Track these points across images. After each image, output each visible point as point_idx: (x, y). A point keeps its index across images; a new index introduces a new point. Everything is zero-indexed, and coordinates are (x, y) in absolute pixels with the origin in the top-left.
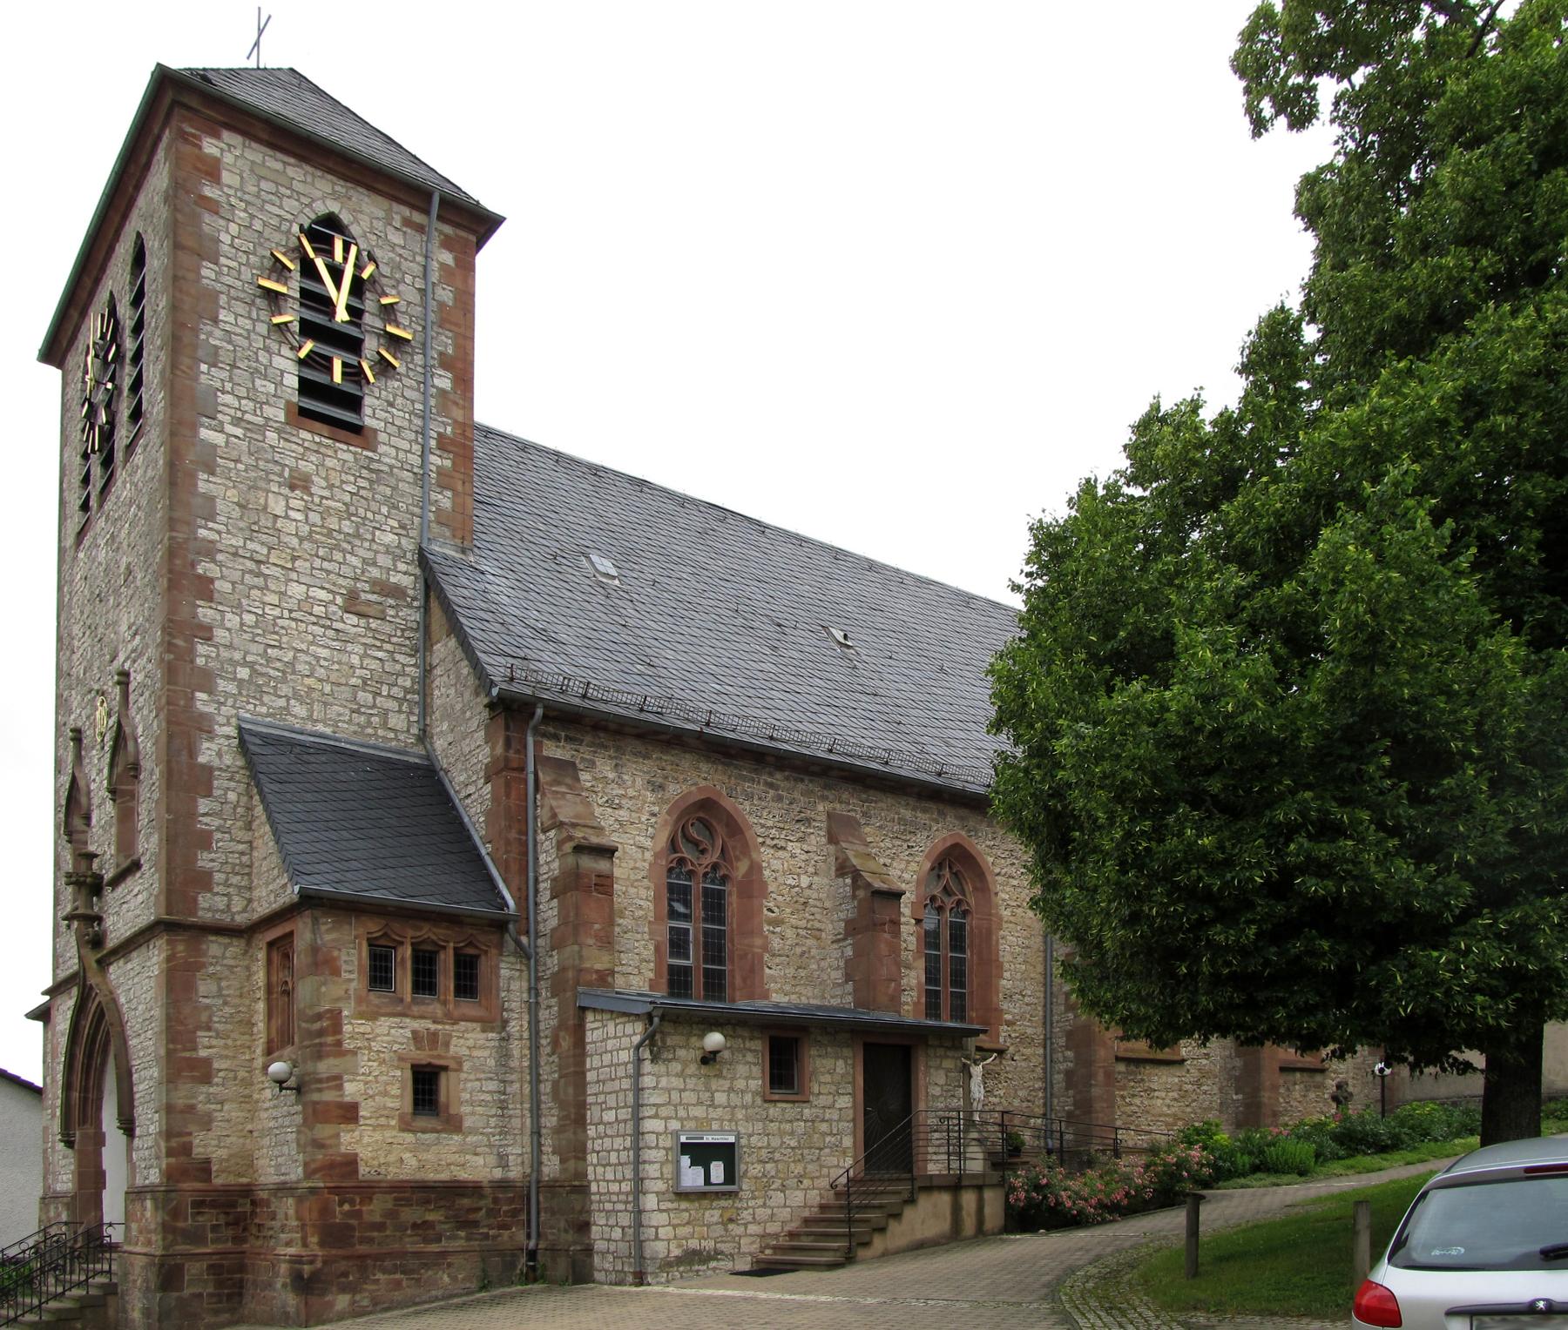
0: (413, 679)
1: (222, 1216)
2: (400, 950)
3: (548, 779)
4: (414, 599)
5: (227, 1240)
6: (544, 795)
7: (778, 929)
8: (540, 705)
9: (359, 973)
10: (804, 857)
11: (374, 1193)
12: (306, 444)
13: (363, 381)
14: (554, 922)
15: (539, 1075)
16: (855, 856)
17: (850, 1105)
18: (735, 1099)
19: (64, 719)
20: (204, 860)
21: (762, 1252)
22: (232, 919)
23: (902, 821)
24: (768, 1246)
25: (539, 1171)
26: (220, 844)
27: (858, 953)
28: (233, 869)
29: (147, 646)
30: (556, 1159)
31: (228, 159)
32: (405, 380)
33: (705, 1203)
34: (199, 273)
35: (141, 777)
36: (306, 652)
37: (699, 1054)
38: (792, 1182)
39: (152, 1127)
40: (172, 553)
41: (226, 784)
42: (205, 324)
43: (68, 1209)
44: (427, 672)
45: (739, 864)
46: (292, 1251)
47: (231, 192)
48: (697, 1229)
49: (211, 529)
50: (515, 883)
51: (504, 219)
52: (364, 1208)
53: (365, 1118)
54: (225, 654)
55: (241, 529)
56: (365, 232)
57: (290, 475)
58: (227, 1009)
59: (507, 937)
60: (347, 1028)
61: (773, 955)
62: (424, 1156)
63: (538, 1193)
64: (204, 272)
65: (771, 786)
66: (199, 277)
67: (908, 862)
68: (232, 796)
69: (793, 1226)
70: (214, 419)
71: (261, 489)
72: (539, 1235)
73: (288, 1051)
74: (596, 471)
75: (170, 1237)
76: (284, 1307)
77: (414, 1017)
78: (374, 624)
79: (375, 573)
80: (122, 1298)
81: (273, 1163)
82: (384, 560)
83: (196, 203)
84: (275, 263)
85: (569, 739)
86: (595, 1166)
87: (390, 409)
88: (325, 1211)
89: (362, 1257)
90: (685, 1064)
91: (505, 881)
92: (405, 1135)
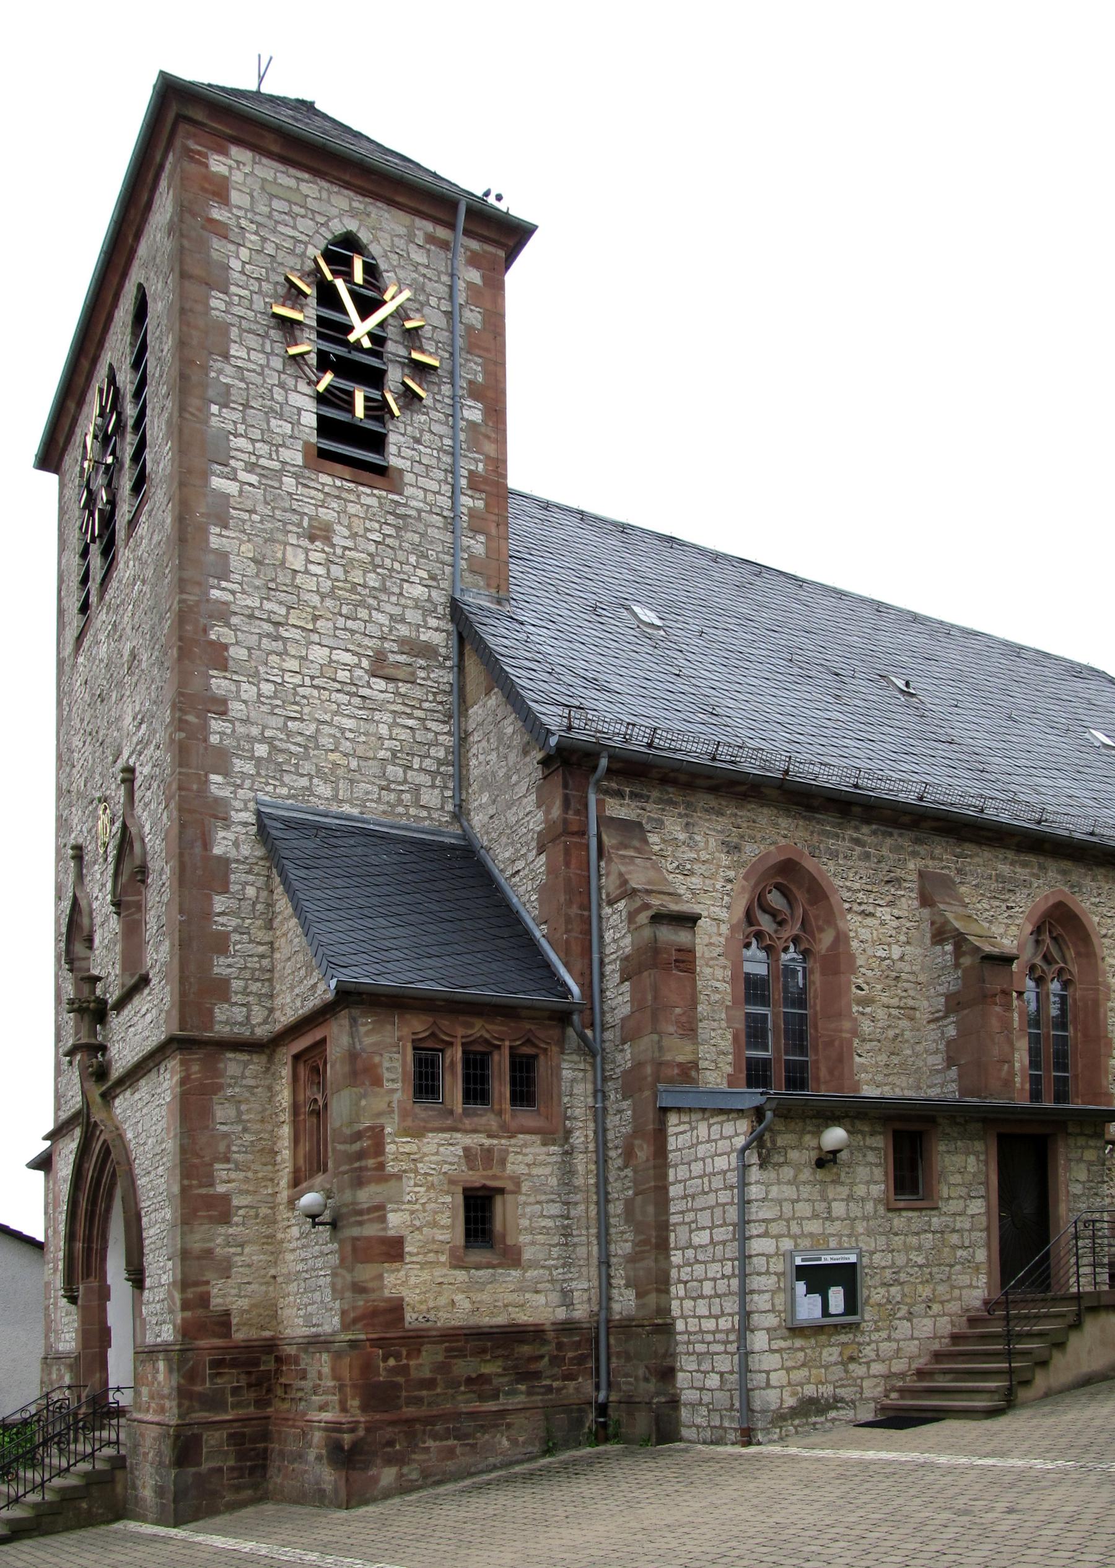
0: (447, 748)
1: (243, 1376)
2: (448, 1053)
3: (614, 842)
4: (446, 658)
5: (249, 1405)
6: (610, 860)
7: (868, 1010)
8: (605, 754)
9: (403, 1081)
10: (895, 923)
11: (422, 1344)
12: (327, 489)
13: (387, 416)
14: (626, 1010)
15: (607, 1193)
16: (956, 919)
17: (983, 1210)
18: (856, 1210)
19: (64, 841)
20: (221, 966)
21: (887, 1396)
22: (252, 1033)
23: (999, 877)
24: (893, 1389)
25: (609, 1309)
26: (238, 947)
27: (963, 1032)
28: (253, 974)
29: (155, 731)
30: (630, 1294)
31: (237, 177)
32: (432, 414)
33: (823, 1338)
34: (207, 305)
35: (149, 881)
36: (329, 724)
37: (814, 1155)
38: (919, 1308)
39: (165, 1277)
40: (183, 616)
41: (244, 877)
42: (215, 361)
43: (71, 1371)
44: (463, 739)
45: (823, 935)
46: (327, 1416)
47: (241, 213)
48: (814, 1371)
49: (224, 589)
50: (578, 966)
51: (536, 227)
52: (411, 1363)
53: (411, 1254)
54: (241, 729)
55: (258, 588)
56: (385, 251)
57: (311, 526)
58: (248, 1137)
59: (570, 1032)
60: (390, 1148)
61: (864, 1040)
62: (478, 1297)
63: (608, 1334)
64: (214, 303)
65: (857, 842)
66: (209, 308)
67: (1008, 925)
68: (251, 892)
69: (920, 1363)
70: (226, 466)
71: (278, 541)
72: (609, 1385)
73: (319, 1179)
74: (623, 528)
75: (186, 1403)
76: (317, 1483)
77: (466, 1132)
78: (403, 688)
79: (404, 630)
80: (132, 1473)
81: (301, 1313)
82: (413, 616)
83: (203, 227)
84: (289, 289)
85: (634, 796)
86: (682, 1299)
87: (416, 446)
88: (367, 1368)
89: (409, 1422)
90: (798, 1168)
91: (566, 965)
92: (457, 1272)
